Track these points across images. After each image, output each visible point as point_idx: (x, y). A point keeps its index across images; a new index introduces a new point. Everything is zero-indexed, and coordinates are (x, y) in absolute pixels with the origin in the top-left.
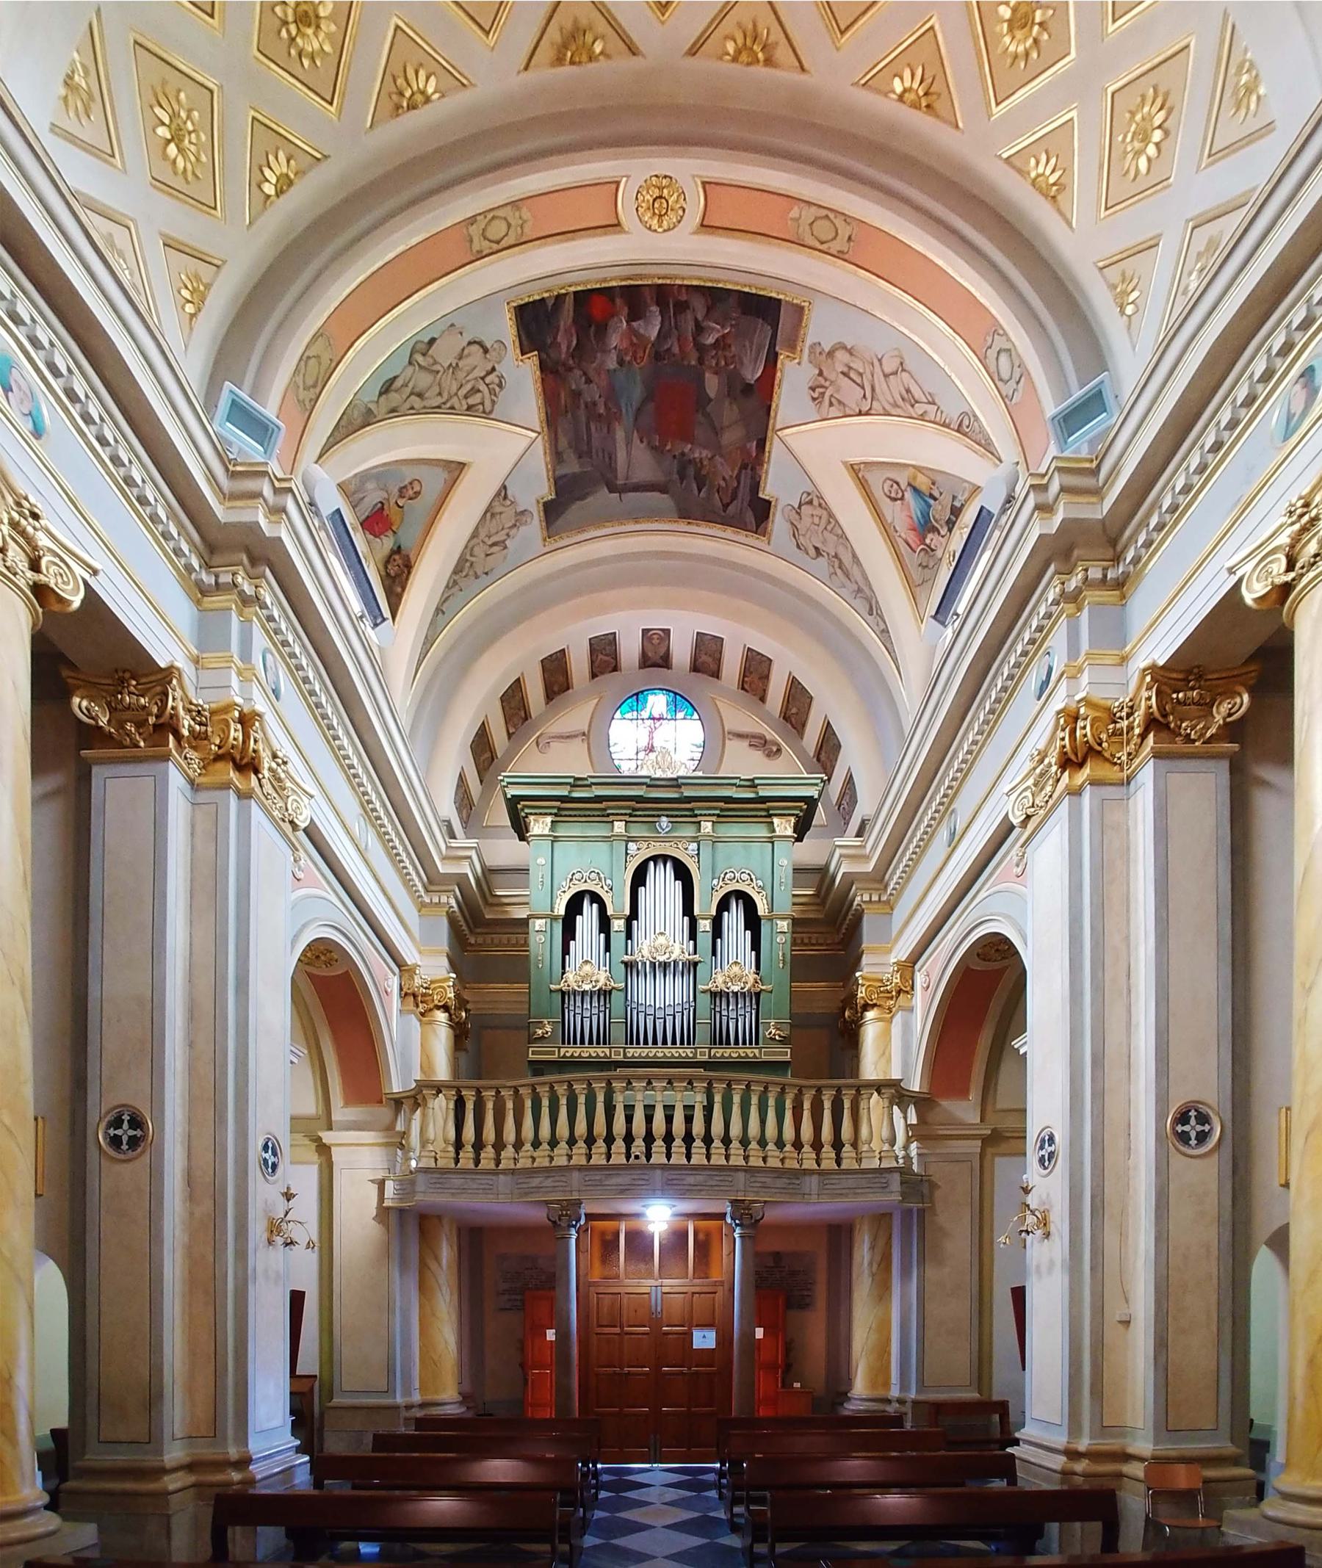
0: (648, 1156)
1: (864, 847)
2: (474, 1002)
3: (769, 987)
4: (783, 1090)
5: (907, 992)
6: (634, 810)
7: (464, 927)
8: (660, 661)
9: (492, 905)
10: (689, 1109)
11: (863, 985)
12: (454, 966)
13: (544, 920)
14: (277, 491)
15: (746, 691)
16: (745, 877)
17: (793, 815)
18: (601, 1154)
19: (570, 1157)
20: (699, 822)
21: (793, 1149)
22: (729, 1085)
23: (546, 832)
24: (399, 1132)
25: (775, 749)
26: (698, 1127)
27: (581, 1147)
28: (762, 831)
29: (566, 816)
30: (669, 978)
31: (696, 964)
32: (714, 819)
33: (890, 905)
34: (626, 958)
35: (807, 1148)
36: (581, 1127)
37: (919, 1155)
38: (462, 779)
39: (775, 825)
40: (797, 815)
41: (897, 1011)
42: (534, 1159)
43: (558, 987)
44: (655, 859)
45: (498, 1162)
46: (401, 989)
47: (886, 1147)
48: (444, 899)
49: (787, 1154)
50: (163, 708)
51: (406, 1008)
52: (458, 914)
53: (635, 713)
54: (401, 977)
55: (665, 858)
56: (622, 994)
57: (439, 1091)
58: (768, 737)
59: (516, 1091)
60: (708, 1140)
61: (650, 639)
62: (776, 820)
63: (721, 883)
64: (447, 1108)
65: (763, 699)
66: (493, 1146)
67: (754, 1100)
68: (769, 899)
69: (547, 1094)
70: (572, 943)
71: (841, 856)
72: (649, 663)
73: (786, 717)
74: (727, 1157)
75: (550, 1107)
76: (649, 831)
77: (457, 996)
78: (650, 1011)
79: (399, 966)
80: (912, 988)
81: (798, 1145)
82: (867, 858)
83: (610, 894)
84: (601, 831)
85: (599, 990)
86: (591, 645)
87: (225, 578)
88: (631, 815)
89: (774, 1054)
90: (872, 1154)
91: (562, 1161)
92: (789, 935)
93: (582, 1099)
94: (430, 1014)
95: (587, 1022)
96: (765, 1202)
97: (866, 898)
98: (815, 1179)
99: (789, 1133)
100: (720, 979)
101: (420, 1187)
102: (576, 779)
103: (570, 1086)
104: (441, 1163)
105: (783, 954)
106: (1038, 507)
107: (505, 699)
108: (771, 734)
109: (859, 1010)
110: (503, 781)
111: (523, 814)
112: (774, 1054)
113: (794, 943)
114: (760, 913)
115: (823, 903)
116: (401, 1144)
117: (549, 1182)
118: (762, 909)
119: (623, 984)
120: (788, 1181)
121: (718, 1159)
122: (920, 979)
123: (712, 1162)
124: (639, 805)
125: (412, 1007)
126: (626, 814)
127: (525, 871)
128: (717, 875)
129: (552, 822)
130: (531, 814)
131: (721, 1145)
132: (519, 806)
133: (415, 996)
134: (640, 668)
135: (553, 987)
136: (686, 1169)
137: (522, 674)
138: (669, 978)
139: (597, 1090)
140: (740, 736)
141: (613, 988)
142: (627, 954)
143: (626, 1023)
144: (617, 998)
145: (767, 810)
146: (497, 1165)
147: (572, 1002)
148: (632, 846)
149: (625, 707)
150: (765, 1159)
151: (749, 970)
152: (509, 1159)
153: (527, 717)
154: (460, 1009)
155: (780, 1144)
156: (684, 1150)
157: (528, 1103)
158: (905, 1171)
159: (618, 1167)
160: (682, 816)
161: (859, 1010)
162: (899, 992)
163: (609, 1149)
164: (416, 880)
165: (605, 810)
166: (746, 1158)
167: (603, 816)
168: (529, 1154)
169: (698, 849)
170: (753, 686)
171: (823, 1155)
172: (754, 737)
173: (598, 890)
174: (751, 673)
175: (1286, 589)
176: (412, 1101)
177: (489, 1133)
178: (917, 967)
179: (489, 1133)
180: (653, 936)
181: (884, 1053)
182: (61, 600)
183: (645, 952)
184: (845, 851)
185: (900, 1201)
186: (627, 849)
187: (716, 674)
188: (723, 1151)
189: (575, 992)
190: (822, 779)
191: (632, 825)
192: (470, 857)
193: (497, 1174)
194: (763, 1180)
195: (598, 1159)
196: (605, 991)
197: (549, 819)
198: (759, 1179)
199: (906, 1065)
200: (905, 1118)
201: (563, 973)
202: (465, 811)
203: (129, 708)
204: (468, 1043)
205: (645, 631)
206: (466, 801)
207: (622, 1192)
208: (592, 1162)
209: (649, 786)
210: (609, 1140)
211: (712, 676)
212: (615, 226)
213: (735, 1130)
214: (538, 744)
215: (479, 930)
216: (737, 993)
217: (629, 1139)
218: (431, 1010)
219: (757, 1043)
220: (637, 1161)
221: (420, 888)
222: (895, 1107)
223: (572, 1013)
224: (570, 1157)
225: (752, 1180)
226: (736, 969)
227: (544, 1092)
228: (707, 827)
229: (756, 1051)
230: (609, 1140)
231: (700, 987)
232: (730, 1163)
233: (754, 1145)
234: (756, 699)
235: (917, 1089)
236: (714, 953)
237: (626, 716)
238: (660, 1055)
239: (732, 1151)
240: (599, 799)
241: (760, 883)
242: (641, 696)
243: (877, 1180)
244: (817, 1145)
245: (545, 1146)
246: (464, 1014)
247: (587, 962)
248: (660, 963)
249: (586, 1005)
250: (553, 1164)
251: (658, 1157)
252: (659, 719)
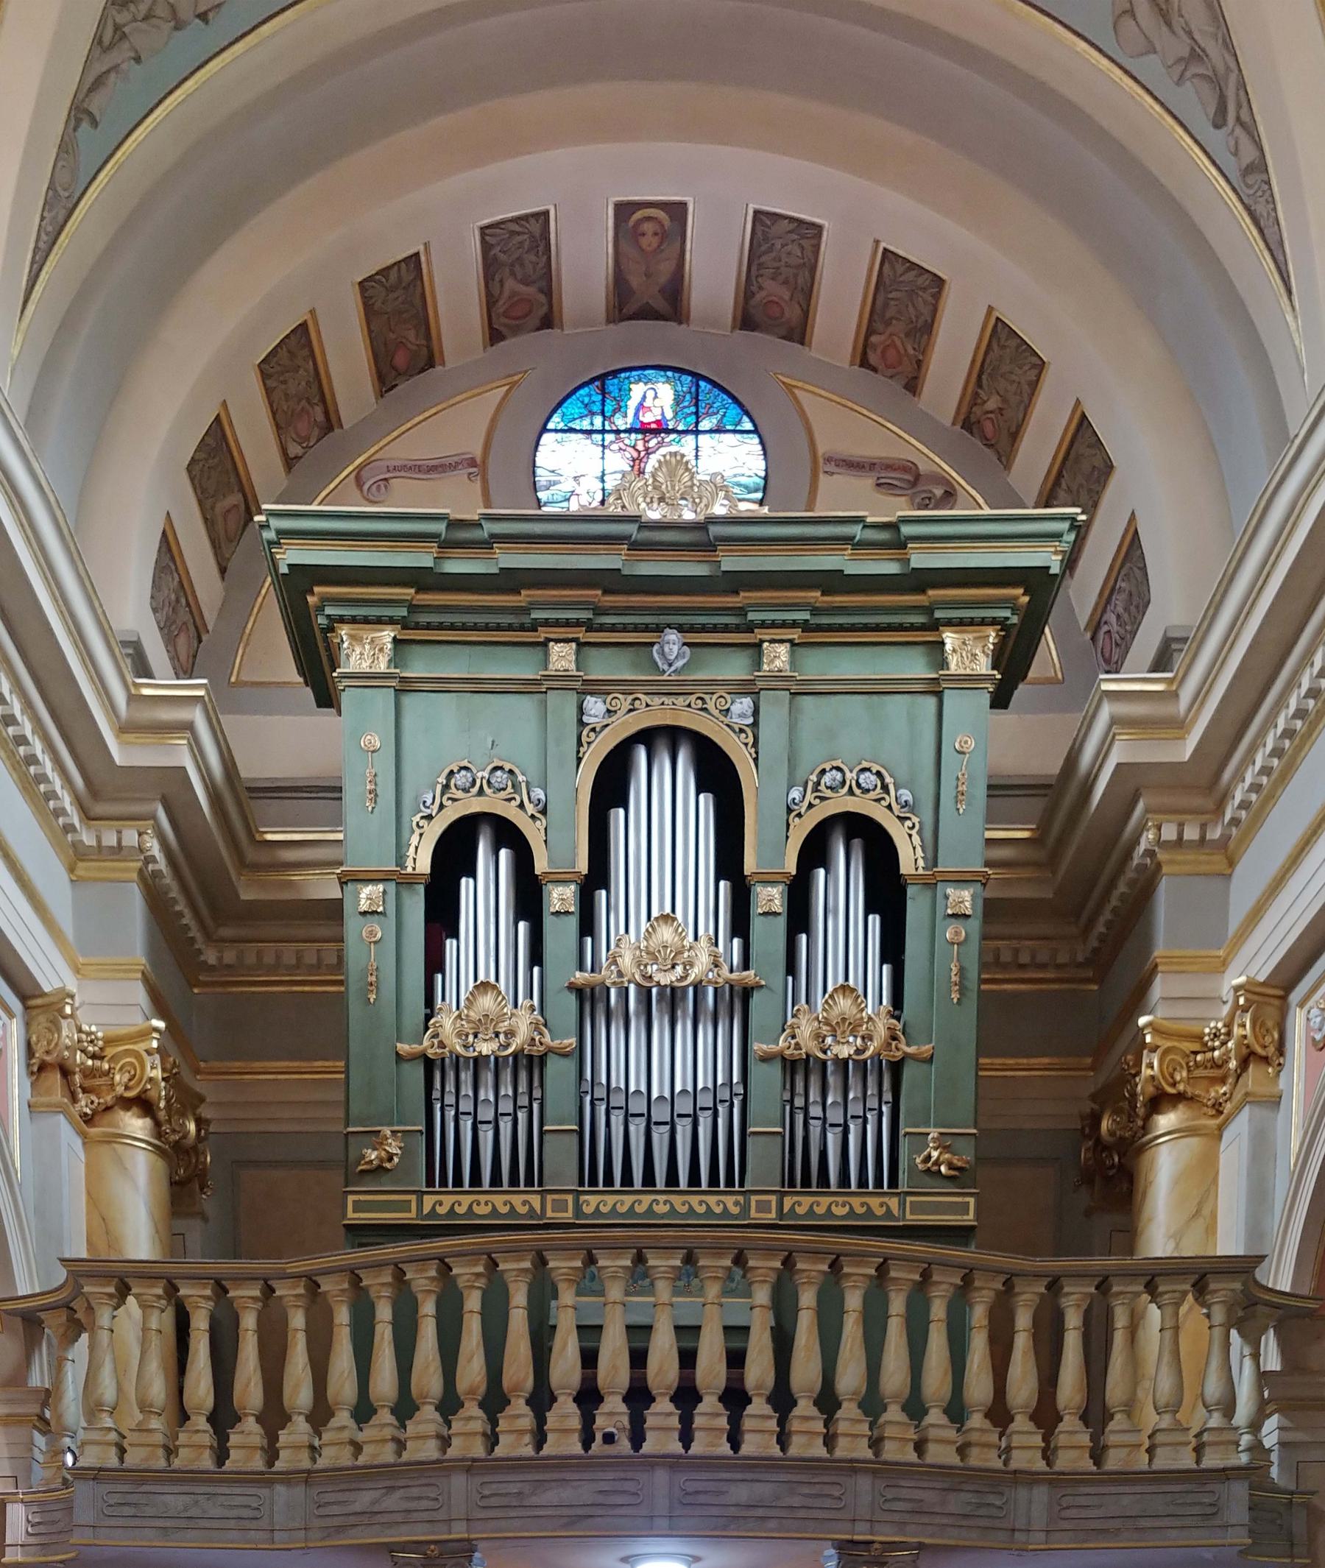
0: (637, 1438)
1: (1175, 695)
2: (219, 1104)
3: (926, 1049)
4: (967, 1281)
5: (1266, 1060)
6: (599, 611)
7: (188, 919)
8: (660, 304)
9: (256, 867)
10: (736, 1332)
11: (1154, 1049)
12: (160, 1005)
13: (381, 887)
15: (875, 370)
16: (868, 780)
17: (994, 622)
18: (521, 1432)
19: (445, 1442)
20: (758, 645)
21: (987, 1424)
22: (835, 1266)
23: (382, 667)
24: (36, 1391)
25: (939, 492)
26: (759, 1370)
27: (471, 1418)
28: (914, 666)
29: (428, 627)
30: (683, 1029)
31: (747, 993)
32: (795, 635)
33: (1228, 853)
34: (580, 977)
35: (1021, 1423)
36: (472, 1370)
37: (1283, 1444)
38: (168, 547)
39: (948, 647)
40: (1001, 623)
41: (1238, 1109)
42: (357, 1448)
43: (416, 1048)
44: (647, 737)
45: (272, 1454)
46: (30, 1051)
47: (1215, 1421)
48: (131, 838)
49: (974, 1437)
51: (44, 1099)
52: (168, 879)
53: (598, 421)
54: (28, 1025)
55: (672, 736)
56: (571, 1065)
57: (123, 1291)
58: (923, 467)
59: (313, 1286)
60: (782, 1400)
61: (637, 234)
62: (950, 639)
63: (809, 797)
64: (145, 1330)
65: (913, 386)
66: (259, 1419)
67: (897, 1304)
68: (928, 834)
69: (386, 1292)
70: (450, 944)
71: (1114, 721)
72: (632, 307)
73: (968, 423)
74: (829, 1440)
75: (395, 1324)
76: (636, 666)
77: (171, 1078)
78: (638, 1106)
79: (23, 998)
80: (1281, 1050)
81: (999, 1414)
82: (1179, 726)
83: (540, 824)
84: (518, 666)
85: (516, 1055)
86: (486, 247)
88: (590, 627)
89: (938, 1209)
90: (1179, 1437)
91: (429, 1451)
92: (975, 925)
93: (473, 1302)
94: (108, 1117)
95: (487, 1136)
96: (921, 1546)
97: (1169, 833)
98: (1041, 1494)
99: (979, 1387)
100: (805, 1030)
101: (84, 1514)
102: (454, 524)
103: (445, 1268)
104: (133, 1459)
105: (962, 971)
107: (269, 369)
108: (930, 460)
109: (1141, 1111)
110: (265, 526)
111: (321, 620)
112: (938, 1209)
113: (990, 963)
114: (906, 867)
115: (1052, 862)
116: (41, 1418)
117: (393, 1501)
118: (910, 859)
119: (572, 1041)
120: (974, 1499)
121: (806, 1445)
122: (1299, 1025)
123: (793, 1451)
124: (610, 600)
125: (58, 1096)
126: (578, 623)
127: (332, 791)
128: (800, 775)
129: (395, 640)
130: (342, 620)
131: (814, 1411)
132: (311, 600)
133: (66, 1072)
134: (610, 320)
135: (404, 1048)
136: (729, 1468)
137: (312, 312)
138: (683, 1029)
139: (509, 1278)
140: (854, 466)
141: (550, 1050)
142: (581, 967)
143: (581, 1133)
144: (559, 1073)
145: (929, 610)
146: (270, 1463)
147: (450, 1087)
148: (595, 706)
149: (572, 407)
150: (920, 1447)
151: (875, 1006)
152: (297, 1448)
153: (330, 423)
154: (183, 1115)
155: (956, 1411)
156: (723, 1422)
157: (343, 1316)
158: (1254, 1473)
159: (563, 1463)
160: (715, 629)
161: (1141, 1111)
162: (1246, 1061)
163: (541, 1420)
164: (57, 784)
165: (525, 611)
166: (876, 1443)
167: (522, 628)
168: (346, 1435)
169: (756, 713)
170: (891, 354)
171: (1061, 1440)
172: (889, 467)
173: (510, 812)
174: (888, 323)
176: (63, 1316)
177: (249, 1387)
178: (1295, 997)
179: (249, 1387)
180: (644, 925)
181: (1197, 1213)
183: (627, 962)
184: (1124, 709)
185: (1244, 1552)
186: (581, 711)
187: (799, 333)
188: (819, 1426)
189: (457, 1061)
190: (1072, 519)
191: (593, 652)
192: (189, 727)
193: (269, 1483)
194: (918, 1494)
195: (514, 1444)
196: (530, 1057)
197: (387, 635)
198: (905, 1493)
199: (1255, 1228)
200: (1256, 1356)
201: (428, 1017)
202: (182, 641)
204: (207, 1202)
205: (623, 210)
206: (184, 615)
207: (574, 1521)
208: (499, 1451)
209: (635, 546)
210: (541, 1399)
211: (788, 337)
213: (850, 1377)
214: (359, 482)
215: (226, 932)
216: (845, 1062)
217: (589, 1397)
218: (108, 1109)
219: (893, 1182)
220: (609, 1450)
221: (67, 802)
222: (1234, 1333)
223: (451, 1113)
224: (445, 1442)
225: (890, 1494)
226: (844, 1004)
227: (379, 1284)
228: (778, 657)
229: (893, 1203)
230: (541, 1399)
231: (757, 1047)
232: (839, 1453)
233: (894, 1413)
234: (897, 386)
235: (1285, 1284)
236: (791, 968)
237: (576, 425)
238: (661, 1209)
239: (842, 1427)
240: (511, 580)
241: (906, 795)
242: (612, 384)
243: (1190, 1499)
244: (1046, 1416)
245: (385, 1416)
246: (192, 1127)
247: (484, 987)
248: (662, 988)
249: (487, 1093)
250: (406, 1456)
251: (663, 1439)
252: (656, 432)
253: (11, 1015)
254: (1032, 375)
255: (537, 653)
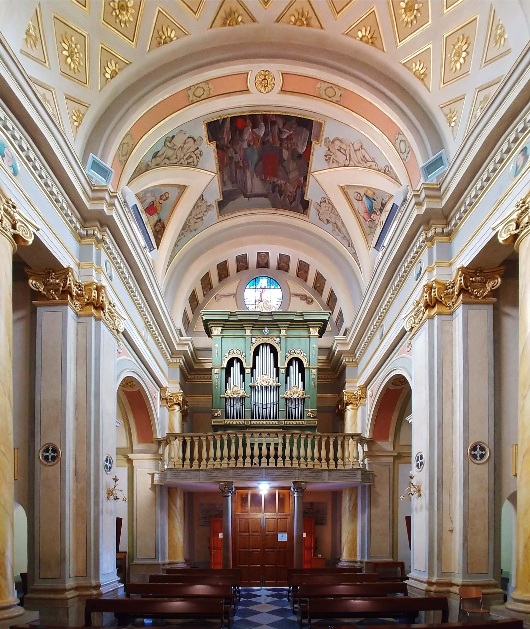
0: (260, 464)
1: (347, 340)
3: (308, 396)
4: (314, 437)
5: (364, 398)
6: (254, 325)
7: (186, 372)
8: (265, 265)
9: (197, 363)
10: (276, 445)
11: (346, 395)
12: (182, 387)
13: (218, 369)
14: (111, 197)
15: (299, 277)
16: (299, 352)
17: (318, 327)
18: (241, 463)
19: (228, 464)
20: (280, 330)
21: (318, 461)
22: (292, 435)
23: (219, 334)
24: (160, 454)
25: (311, 300)
26: (280, 452)
27: (233, 460)
28: (305, 334)
29: (227, 327)
30: (268, 392)
31: (279, 387)
32: (286, 328)
33: (357, 363)
34: (251, 384)
35: (323, 461)
36: (233, 452)
37: (368, 463)
38: (185, 312)
39: (311, 331)
40: (319, 327)
41: (360, 406)
42: (214, 465)
43: (224, 396)
44: (262, 344)
45: (200, 466)
46: (161, 397)
47: (355, 460)
48: (178, 361)
49: (315, 463)
50: (65, 284)
51: (163, 404)
52: (184, 367)
53: (255, 286)
54: (161, 392)
55: (267, 344)
56: (249, 399)
57: (176, 438)
58: (308, 296)
59: (207, 438)
60: (284, 457)
61: (261, 256)
62: (311, 329)
63: (289, 354)
64: (179, 445)
65: (306, 281)
66: (198, 460)
67: (302, 441)
68: (308, 361)
69: (219, 439)
70: (229, 378)
71: (337, 343)
72: (260, 266)
74: (292, 464)
75: (220, 444)
76: (260, 333)
77: (183, 400)
78: (261, 406)
79: (160, 388)
80: (366, 396)
81: (320, 459)
82: (347, 344)
83: (245, 359)
84: (241, 333)
85: (240, 397)
86: (237, 259)
87: (90, 232)
88: (253, 327)
89: (310, 423)
90: (349, 463)
91: (225, 466)
92: (316, 375)
93: (233, 441)
94: (172, 407)
95: (235, 410)
96: (307, 482)
97: (347, 360)
98: (327, 473)
99: (316, 455)
100: (289, 393)
101: (169, 476)
102: (231, 313)
103: (229, 436)
104: (177, 467)
105: (314, 383)
106: (416, 204)
107: (202, 280)
108: (309, 295)
109: (345, 405)
110: (201, 313)
111: (210, 327)
112: (310, 423)
113: (318, 378)
114: (305, 366)
115: (330, 362)
116: (161, 459)
117: (220, 474)
118: (305, 365)
119: (250, 395)
120: (316, 474)
121: (288, 465)
122: (369, 393)
123: (285, 466)
124: (256, 323)
125: (165, 404)
126: (251, 327)
127: (210, 349)
128: (287, 351)
129: (221, 330)
130: (213, 326)
131: (289, 459)
132: (208, 323)
133: (166, 399)
134: (257, 268)
135: (222, 396)
136: (275, 469)
137: (209, 270)
138: (268, 392)
139: (239, 437)
140: (297, 295)
141: (246, 396)
142: (251, 383)
143: (251, 410)
144: (247, 400)
145: (308, 325)
146: (199, 467)
147: (229, 402)
148: (253, 339)
149: (250, 284)
150: (307, 465)
151: (300, 389)
152: (204, 465)
153: (211, 288)
154: (184, 405)
155: (313, 459)
156: (274, 461)
157: (212, 443)
159: (248, 468)
160: (273, 327)
161: (345, 405)
162: (361, 398)
163: (244, 461)
164: (167, 353)
165: (242, 325)
166: (299, 465)
167: (242, 327)
168: (212, 463)
169: (280, 341)
170: (302, 275)
171: (330, 463)
172: (302, 295)
173: (240, 357)
174: (301, 270)
175: (516, 236)
176: (165, 442)
177: (196, 455)
178: (368, 388)
179: (196, 455)
180: (262, 375)
181: (354, 423)
182: (24, 241)
183: (259, 382)
184: (339, 342)
185: (361, 482)
186: (251, 341)
187: (287, 270)
188: (290, 462)
189: (230, 398)
190: (329, 312)
191: (253, 331)
192: (188, 344)
193: (199, 471)
194: (306, 473)
195: (240, 465)
196: (243, 398)
197: (220, 329)
198: (304, 473)
199: (363, 427)
200: (363, 449)
201: (226, 390)
202: (186, 326)
203: (52, 284)
204: (188, 419)
205: (259, 253)
206: (187, 321)
207: (249, 478)
208: (237, 466)
209: (260, 315)
210: (244, 457)
211: (286, 271)
212: (247, 91)
213: (295, 453)
214: (216, 299)
215: (192, 373)
216: (295, 398)
217: (252, 457)
218: (173, 405)
219: (303, 418)
220: (255, 466)
221: (169, 356)
222: (359, 444)
223: (229, 407)
224: (228, 464)
225: (302, 473)
226: (295, 389)
227: (218, 438)
228: (283, 332)
229: (303, 422)
230: (244, 457)
231: (281, 396)
232: (293, 467)
233: (302, 459)
234: (303, 280)
235: (368, 437)
236: (286, 382)
237: (251, 287)
238: (265, 423)
239: (294, 462)
240: (240, 321)
241: (305, 354)
242: (257, 279)
243: (351, 473)
244: (328, 459)
245: (219, 460)
246: (186, 407)
247: (235, 386)
248: (265, 386)
249: (235, 403)
250: (222, 467)
251: (264, 464)
252: (264, 289)
253: (158, 391)
254: (324, 281)
255: (244, 331)
